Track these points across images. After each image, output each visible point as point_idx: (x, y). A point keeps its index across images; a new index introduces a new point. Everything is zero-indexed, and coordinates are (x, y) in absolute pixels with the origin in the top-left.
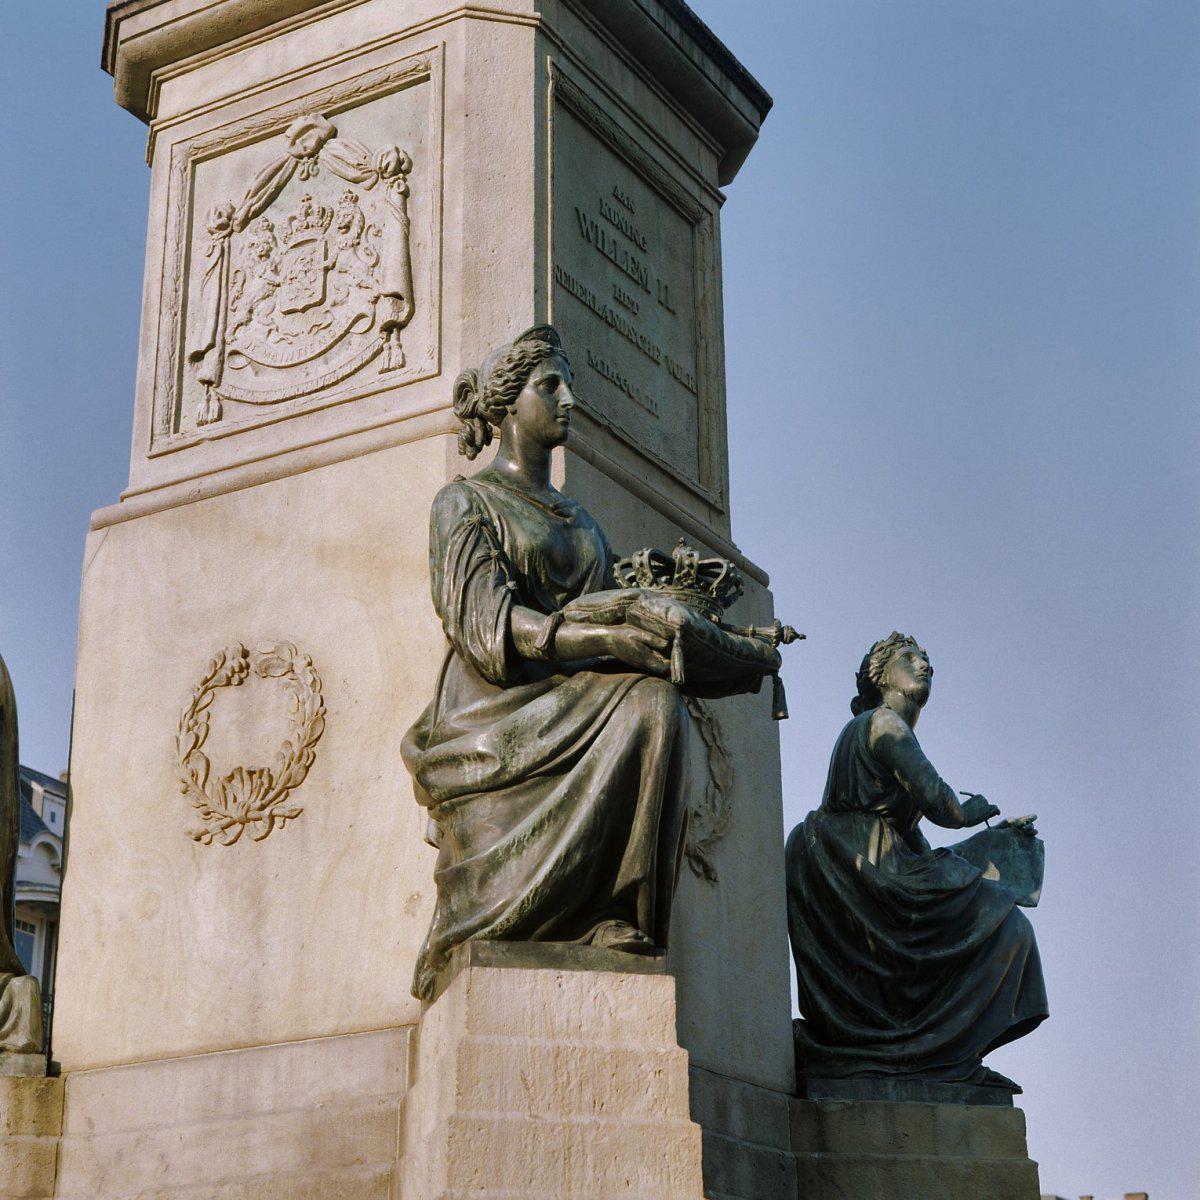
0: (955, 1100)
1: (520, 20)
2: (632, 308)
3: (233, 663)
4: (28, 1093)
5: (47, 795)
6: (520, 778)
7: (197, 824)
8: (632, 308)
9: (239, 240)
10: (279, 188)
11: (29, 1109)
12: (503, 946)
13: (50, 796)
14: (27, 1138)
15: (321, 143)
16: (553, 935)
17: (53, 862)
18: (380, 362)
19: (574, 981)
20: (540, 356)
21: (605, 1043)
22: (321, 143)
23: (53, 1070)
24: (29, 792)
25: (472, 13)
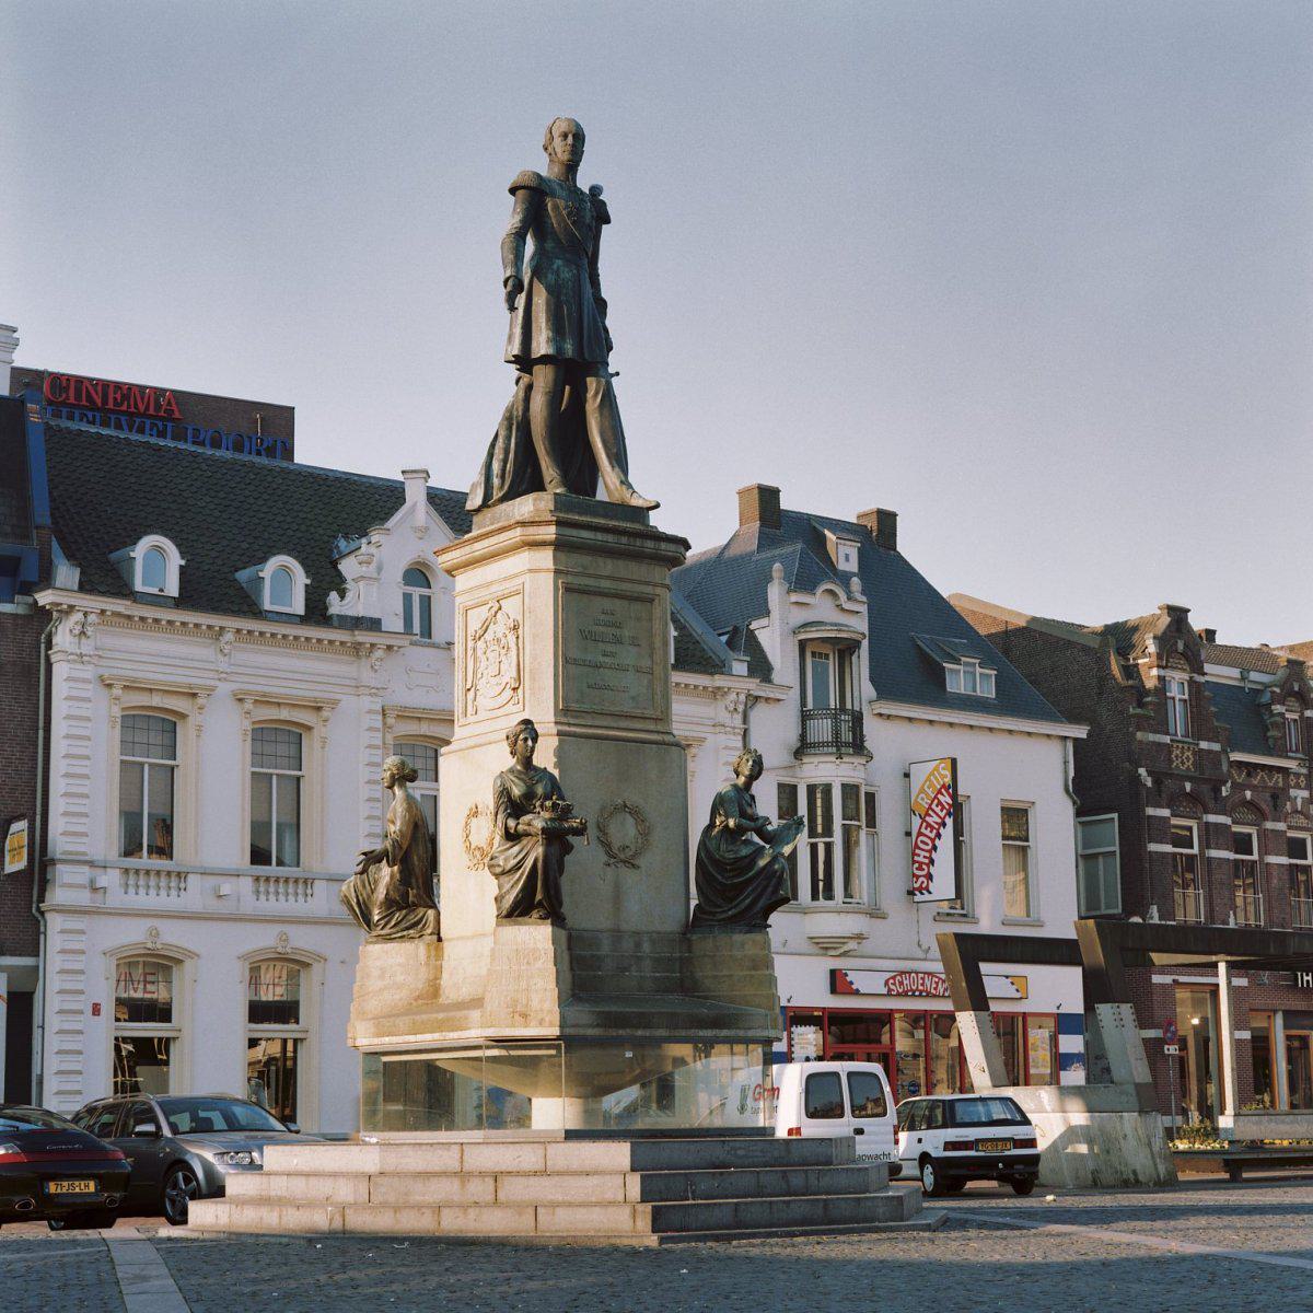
0: (740, 932)
1: (548, 570)
2: (613, 655)
3: (474, 810)
4: (432, 948)
5: (839, 541)
6: (510, 871)
7: (469, 863)
8: (613, 655)
9: (479, 643)
10: (488, 627)
11: (433, 953)
12: (504, 920)
13: (842, 541)
14: (432, 962)
15: (496, 613)
16: (520, 915)
17: (837, 603)
18: (512, 702)
19: (524, 929)
20: (521, 732)
21: (531, 946)
22: (496, 613)
23: (440, 940)
24: (822, 540)
25: (530, 571)
